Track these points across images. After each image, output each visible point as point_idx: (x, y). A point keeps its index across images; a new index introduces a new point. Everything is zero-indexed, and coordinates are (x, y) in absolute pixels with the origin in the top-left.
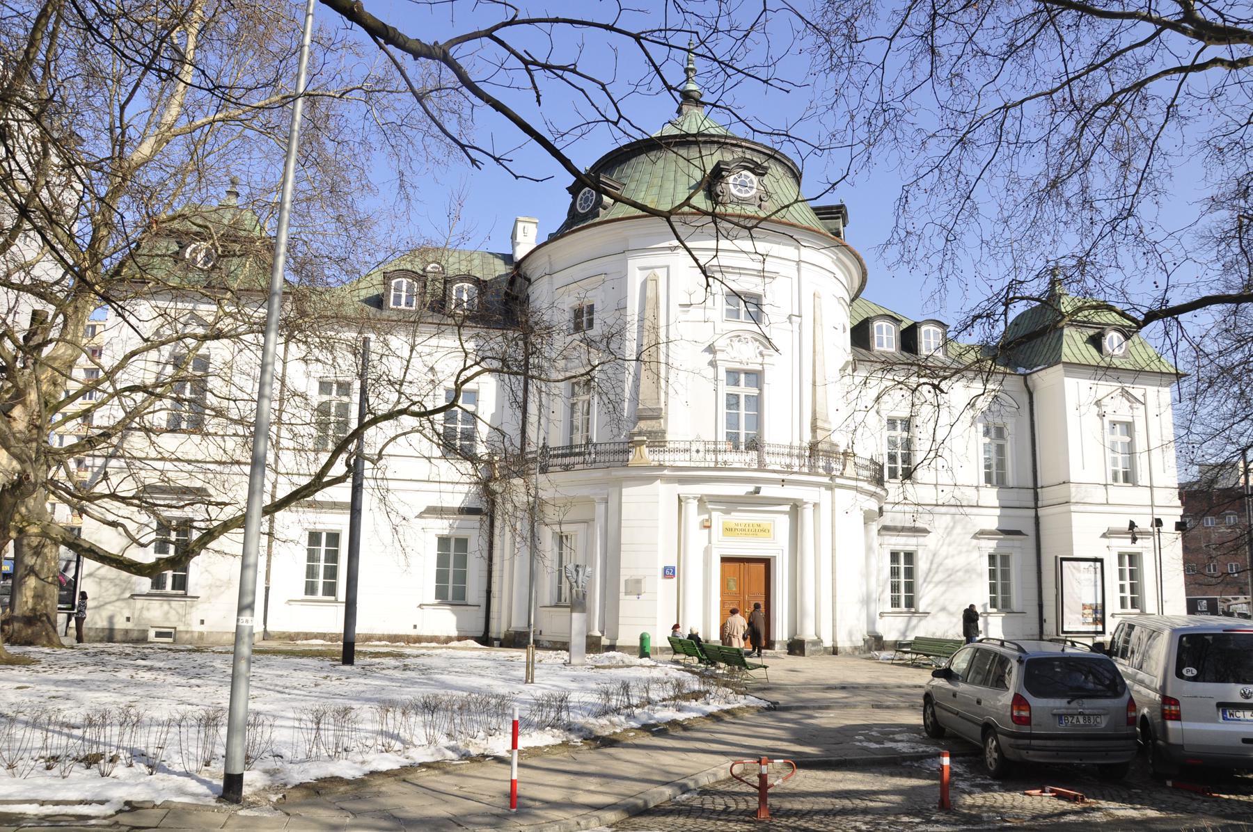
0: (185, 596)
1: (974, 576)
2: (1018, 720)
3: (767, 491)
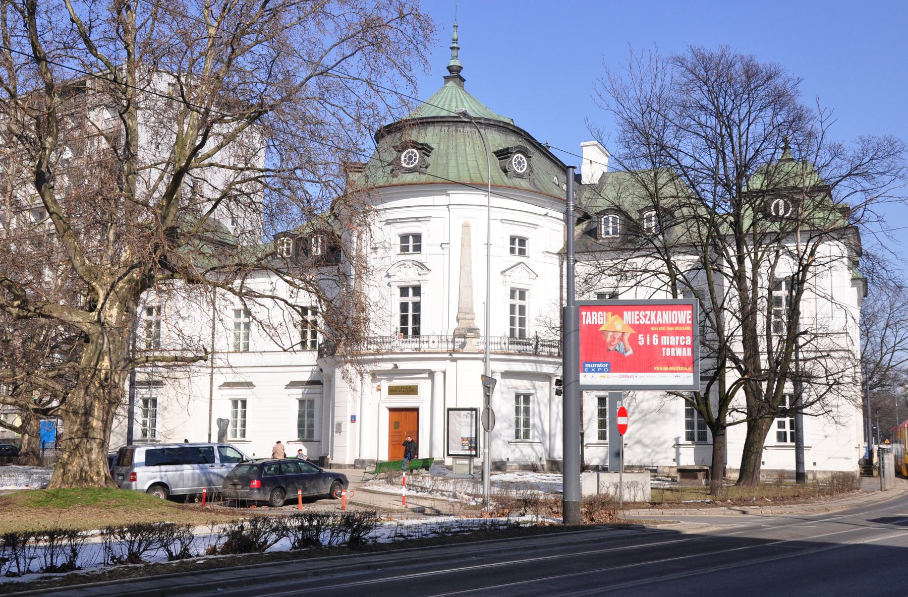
1: (667, 416)
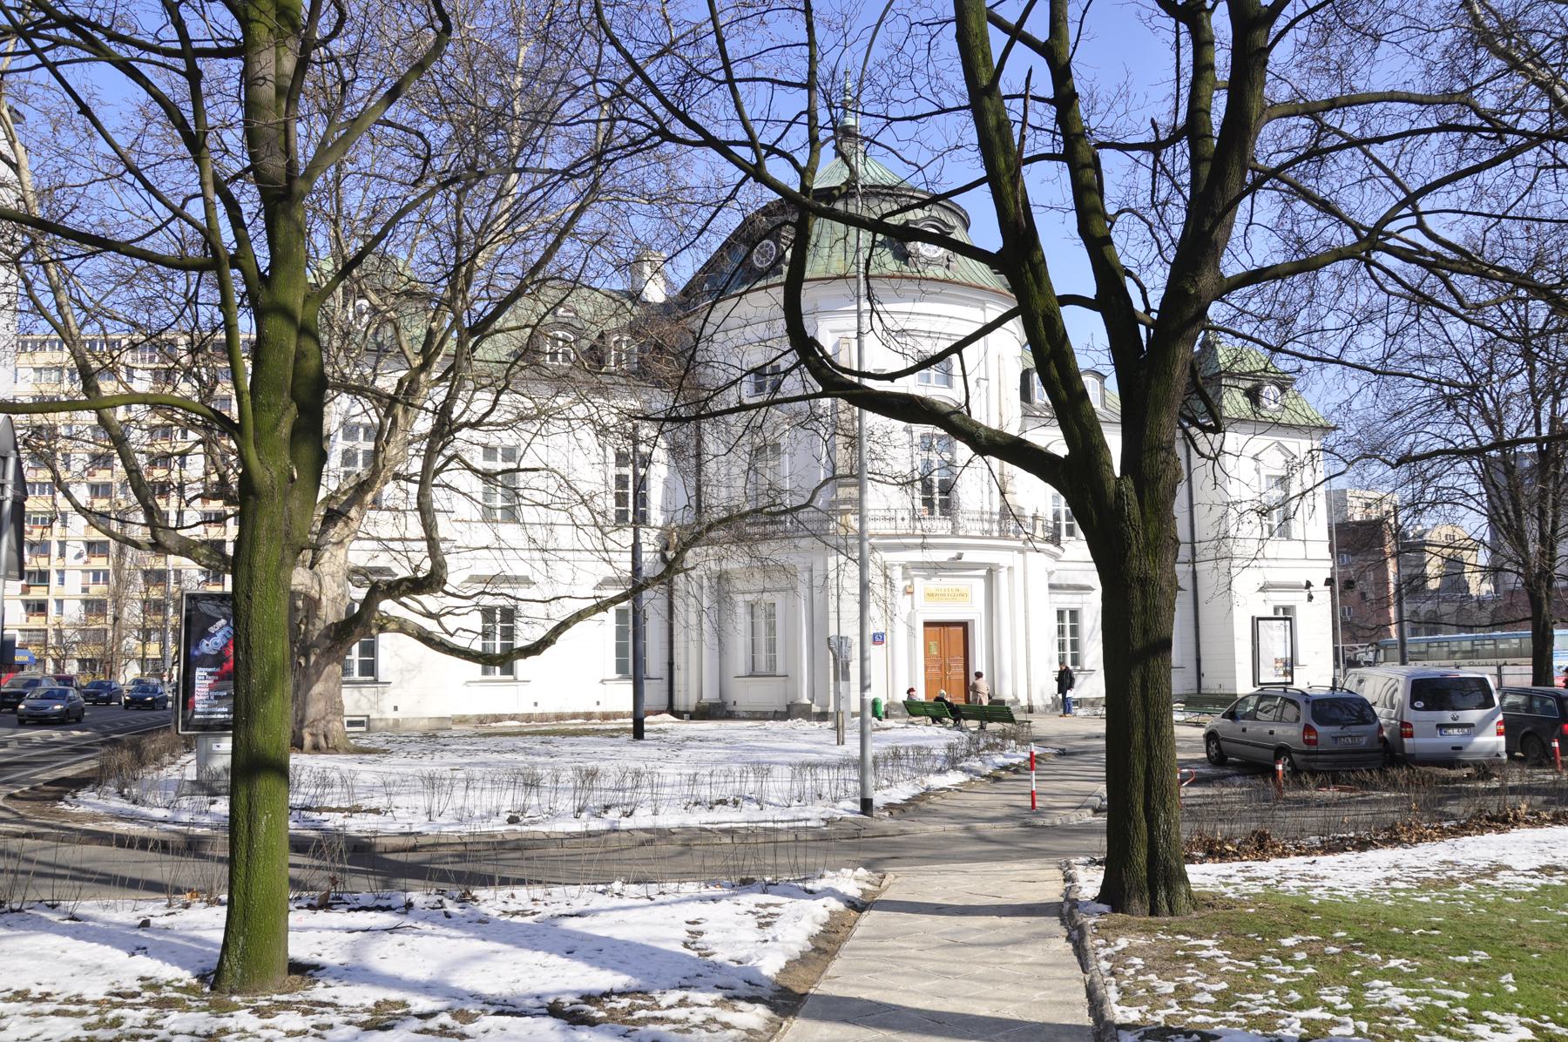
0: (376, 681)
2: (1308, 742)
3: (969, 556)
